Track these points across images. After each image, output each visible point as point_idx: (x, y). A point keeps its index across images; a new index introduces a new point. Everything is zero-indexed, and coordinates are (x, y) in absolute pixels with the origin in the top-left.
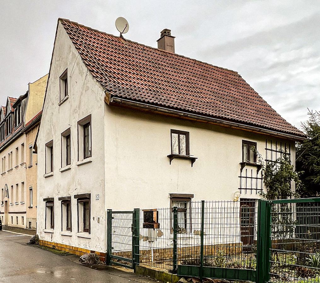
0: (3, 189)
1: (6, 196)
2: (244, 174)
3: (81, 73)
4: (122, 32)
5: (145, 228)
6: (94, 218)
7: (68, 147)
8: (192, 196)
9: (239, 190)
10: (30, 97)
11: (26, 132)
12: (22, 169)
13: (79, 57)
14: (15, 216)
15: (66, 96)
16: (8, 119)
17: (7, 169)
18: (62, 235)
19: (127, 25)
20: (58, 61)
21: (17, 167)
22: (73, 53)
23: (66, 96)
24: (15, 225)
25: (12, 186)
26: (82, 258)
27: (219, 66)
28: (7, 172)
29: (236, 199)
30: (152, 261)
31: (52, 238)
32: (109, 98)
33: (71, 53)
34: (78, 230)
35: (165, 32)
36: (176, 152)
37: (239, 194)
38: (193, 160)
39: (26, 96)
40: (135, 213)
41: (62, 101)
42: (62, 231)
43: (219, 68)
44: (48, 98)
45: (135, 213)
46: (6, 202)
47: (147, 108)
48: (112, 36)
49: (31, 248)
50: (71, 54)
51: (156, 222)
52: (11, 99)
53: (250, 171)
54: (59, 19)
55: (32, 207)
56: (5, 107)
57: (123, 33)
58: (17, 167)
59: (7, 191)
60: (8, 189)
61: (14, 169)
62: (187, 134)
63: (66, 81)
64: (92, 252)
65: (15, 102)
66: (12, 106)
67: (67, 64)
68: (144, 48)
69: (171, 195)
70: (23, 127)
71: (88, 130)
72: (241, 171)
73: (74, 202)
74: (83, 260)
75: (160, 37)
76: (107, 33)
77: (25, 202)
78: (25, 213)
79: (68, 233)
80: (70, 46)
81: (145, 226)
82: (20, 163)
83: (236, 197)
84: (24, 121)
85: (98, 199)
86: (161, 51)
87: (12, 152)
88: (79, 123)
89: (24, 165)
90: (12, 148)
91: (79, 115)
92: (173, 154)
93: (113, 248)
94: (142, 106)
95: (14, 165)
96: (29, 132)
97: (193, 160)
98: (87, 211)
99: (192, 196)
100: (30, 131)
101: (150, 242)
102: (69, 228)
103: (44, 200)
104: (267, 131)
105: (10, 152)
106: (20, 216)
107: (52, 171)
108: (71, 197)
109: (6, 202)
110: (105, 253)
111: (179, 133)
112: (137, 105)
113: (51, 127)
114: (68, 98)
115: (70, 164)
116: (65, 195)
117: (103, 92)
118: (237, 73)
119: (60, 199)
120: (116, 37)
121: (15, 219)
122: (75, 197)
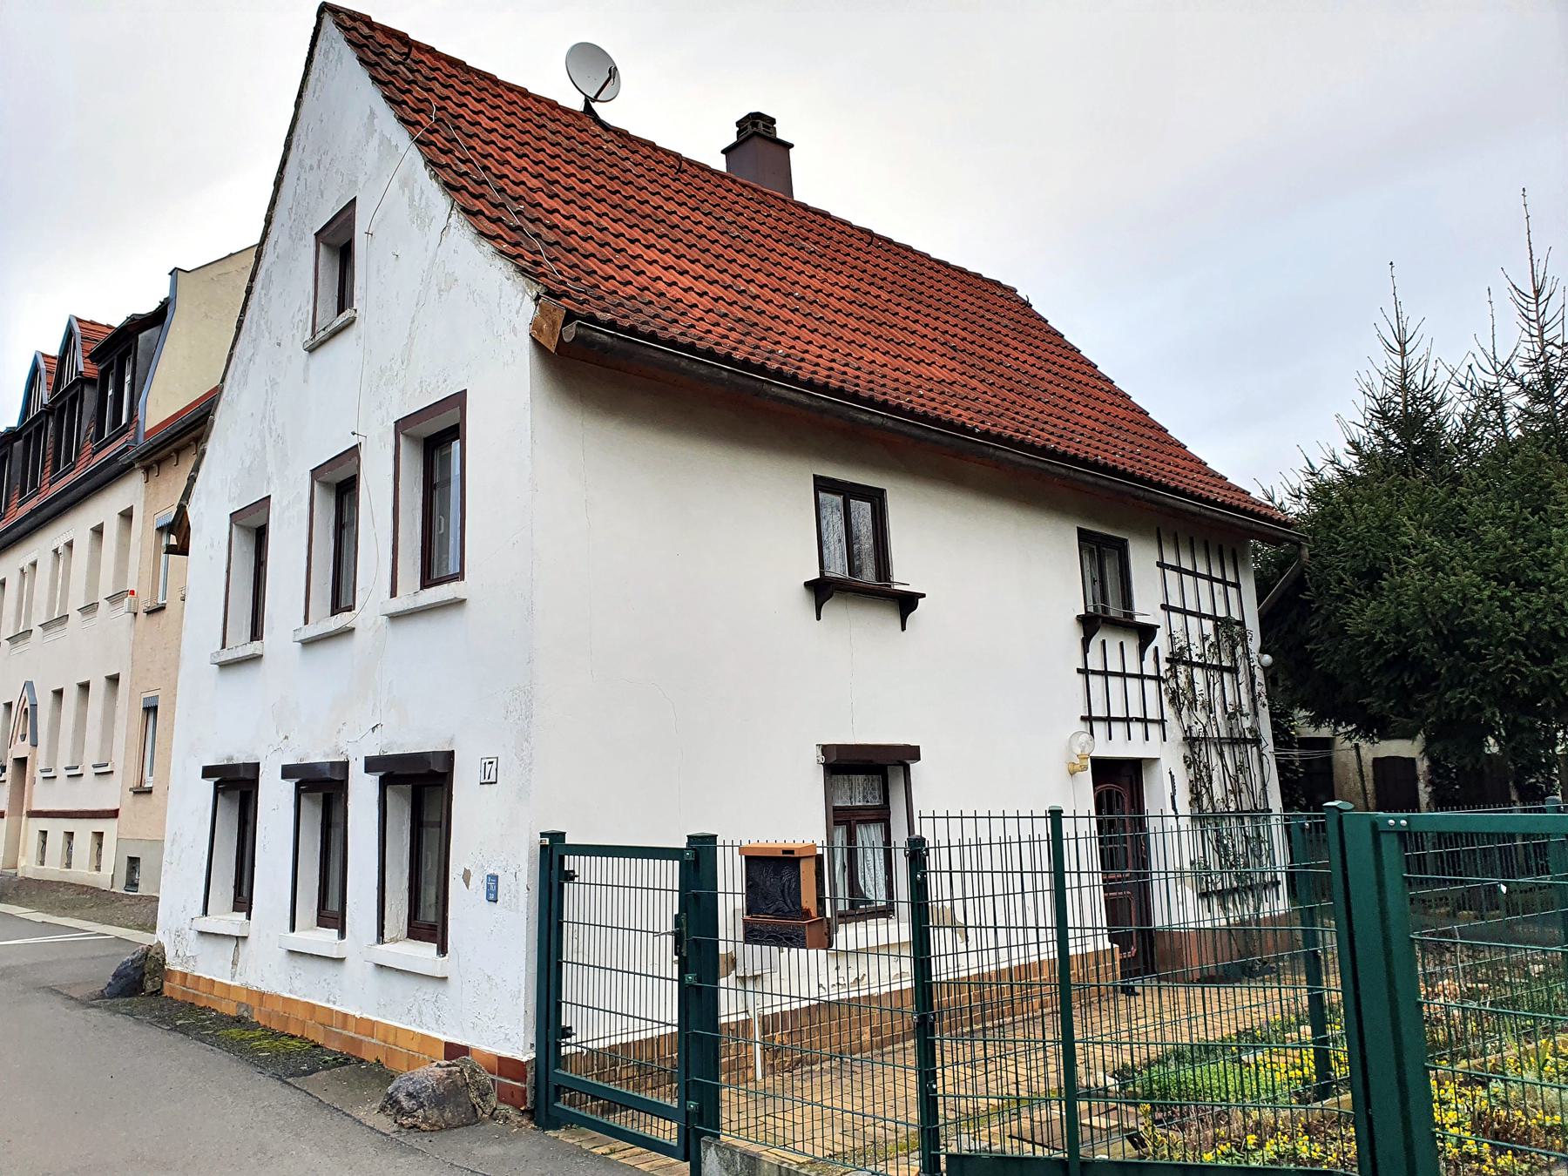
0: (9, 706)
1: (23, 737)
2: (1095, 663)
3: (421, 217)
4: (592, 96)
5: (756, 942)
6: (467, 876)
7: (436, 494)
8: (913, 753)
9: (1084, 727)
10: (178, 325)
11: (147, 462)
12: (115, 619)
13: (415, 158)
14: (57, 828)
15: (341, 309)
16: (64, 405)
17: (41, 616)
18: (291, 952)
19: (613, 73)
20: (311, 168)
21: (89, 609)
22: (385, 141)
23: (341, 309)
24: (53, 869)
25: (59, 694)
26: (401, 1097)
27: (952, 262)
28: (37, 631)
29: (1077, 761)
30: (759, 1077)
31: (234, 963)
32: (554, 323)
33: (376, 135)
34: (381, 933)
35: (755, 125)
36: (838, 569)
37: (1087, 736)
38: (906, 603)
39: (159, 317)
40: (697, 862)
41: (322, 334)
42: (293, 929)
43: (954, 270)
44: (255, 318)
45: (697, 862)
46: (21, 762)
47: (722, 381)
48: (553, 105)
49: (123, 1026)
50: (375, 142)
51: (814, 913)
52: (83, 325)
53: (1116, 650)
54: (324, 9)
55: (149, 791)
56: (54, 358)
57: (595, 99)
58: (89, 609)
59: (31, 713)
60: (34, 706)
61: (75, 616)
62: (877, 499)
63: (345, 254)
64: (454, 1051)
65: (102, 338)
66: (87, 355)
67: (355, 182)
68: (680, 165)
69: (825, 749)
70: (136, 439)
71: (447, 460)
72: (1086, 650)
73: (363, 792)
74: (405, 1104)
75: (733, 139)
76: (530, 91)
77: (117, 764)
78: (114, 814)
79: (323, 941)
80: (371, 109)
81: (753, 935)
82: (106, 588)
83: (1079, 753)
84: (140, 417)
85: (493, 779)
86: (744, 186)
87: (72, 541)
88: (402, 426)
89: (126, 600)
90: (76, 526)
91: (403, 392)
92: (827, 574)
93: (567, 1032)
94: (703, 371)
95: (77, 599)
96: (159, 463)
97: (906, 603)
98: (430, 837)
99: (913, 753)
100: (168, 457)
101: (744, 979)
102: (332, 916)
103: (208, 772)
104: (1168, 500)
105: (60, 543)
106: (84, 830)
107: (256, 633)
108: (347, 763)
109: (21, 762)
110: (525, 1059)
111: (849, 492)
112: (684, 363)
113: (263, 442)
114: (352, 321)
115: (350, 609)
116: (318, 754)
117: (527, 298)
118: (1014, 291)
119: (287, 772)
120: (567, 111)
121: (56, 843)
122: (371, 765)
